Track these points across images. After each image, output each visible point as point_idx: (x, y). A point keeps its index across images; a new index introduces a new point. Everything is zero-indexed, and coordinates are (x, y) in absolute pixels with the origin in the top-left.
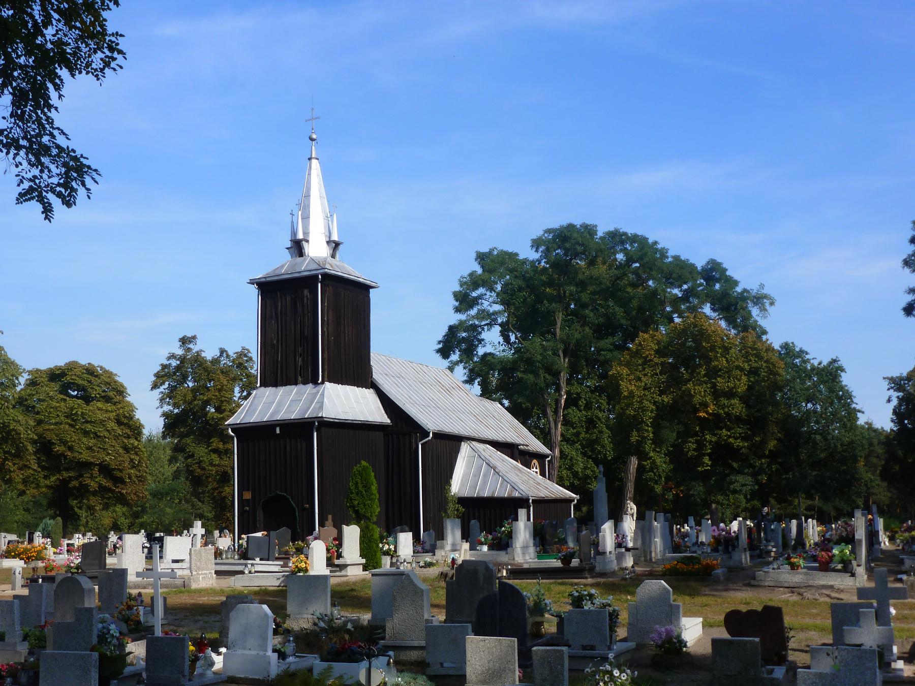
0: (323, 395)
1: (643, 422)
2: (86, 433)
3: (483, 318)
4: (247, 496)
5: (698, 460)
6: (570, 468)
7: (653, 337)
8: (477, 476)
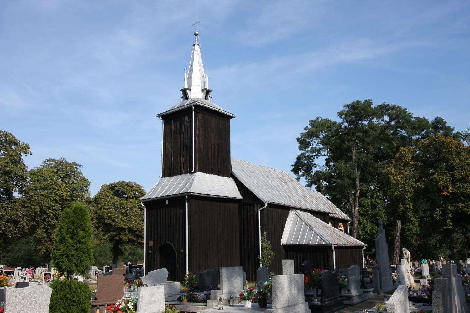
0: (193, 179)
1: (406, 199)
2: (122, 213)
3: (314, 152)
4: (151, 244)
5: (444, 221)
6: (364, 229)
7: (409, 149)
8: (298, 231)
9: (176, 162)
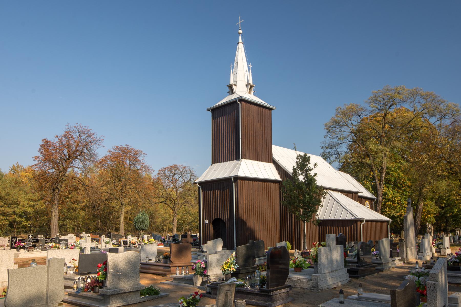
9: (227, 146)
